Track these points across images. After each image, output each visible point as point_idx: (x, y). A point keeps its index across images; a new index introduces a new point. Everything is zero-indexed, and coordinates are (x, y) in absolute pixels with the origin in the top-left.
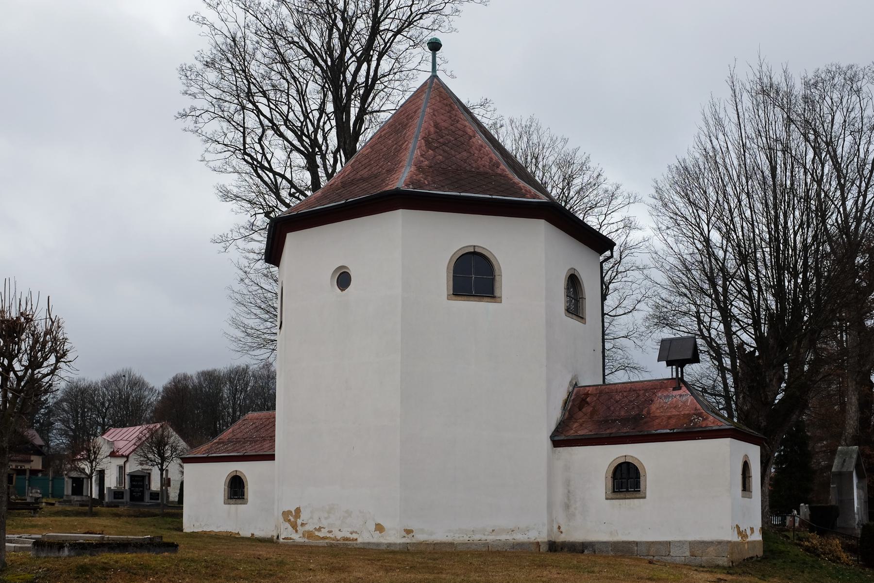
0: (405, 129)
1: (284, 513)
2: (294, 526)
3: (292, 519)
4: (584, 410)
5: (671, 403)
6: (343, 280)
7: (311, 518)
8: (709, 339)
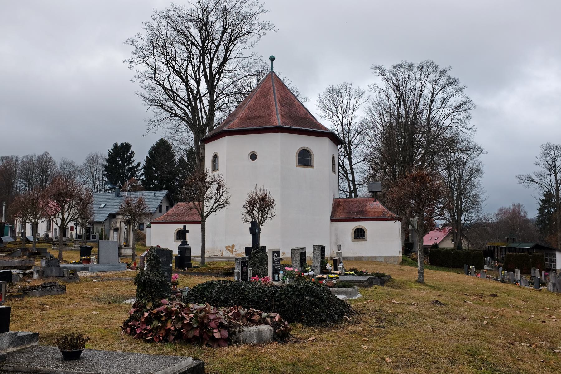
0: (268, 95)
1: (226, 247)
2: (232, 252)
3: (230, 249)
4: (339, 208)
5: (374, 207)
6: (253, 157)
7: (240, 249)
8: (343, 167)
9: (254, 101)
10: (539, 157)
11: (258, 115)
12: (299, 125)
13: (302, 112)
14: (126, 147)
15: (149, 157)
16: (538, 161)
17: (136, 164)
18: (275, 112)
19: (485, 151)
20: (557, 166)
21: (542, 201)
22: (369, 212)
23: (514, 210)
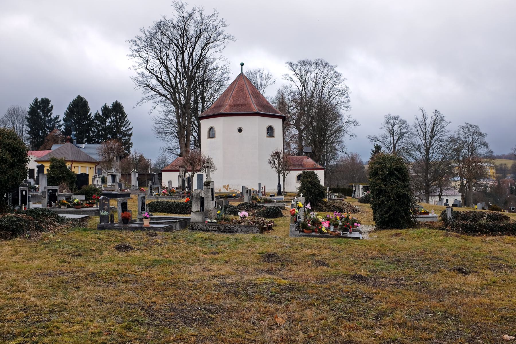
2: (227, 189)
6: (240, 130)
9: (236, 94)
10: (384, 124)
11: (240, 103)
12: (267, 112)
13: (265, 102)
14: (46, 102)
15: (67, 111)
16: (382, 126)
17: (55, 117)
18: (251, 102)
19: (359, 124)
20: (394, 130)
21: (373, 151)
22: (306, 165)
23: (352, 158)
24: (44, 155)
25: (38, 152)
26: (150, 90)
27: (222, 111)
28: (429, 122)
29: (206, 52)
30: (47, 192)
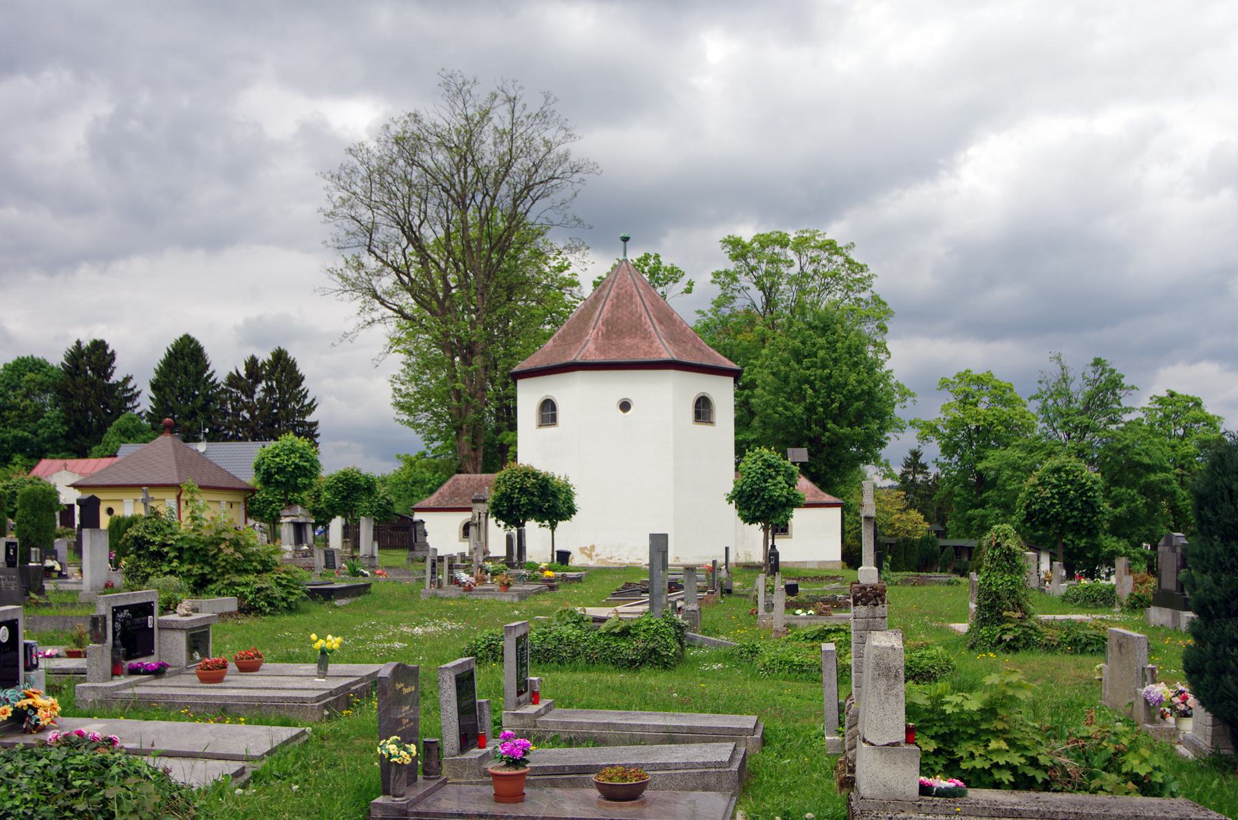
2: (590, 556)
6: (625, 406)
24: (97, 470)
25: (82, 462)
26: (377, 304)
27: (575, 356)
28: (1079, 390)
29: (527, 206)
30: (110, 617)
